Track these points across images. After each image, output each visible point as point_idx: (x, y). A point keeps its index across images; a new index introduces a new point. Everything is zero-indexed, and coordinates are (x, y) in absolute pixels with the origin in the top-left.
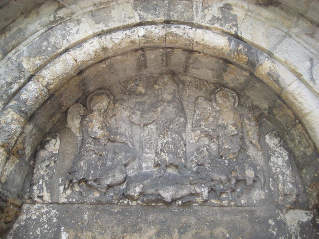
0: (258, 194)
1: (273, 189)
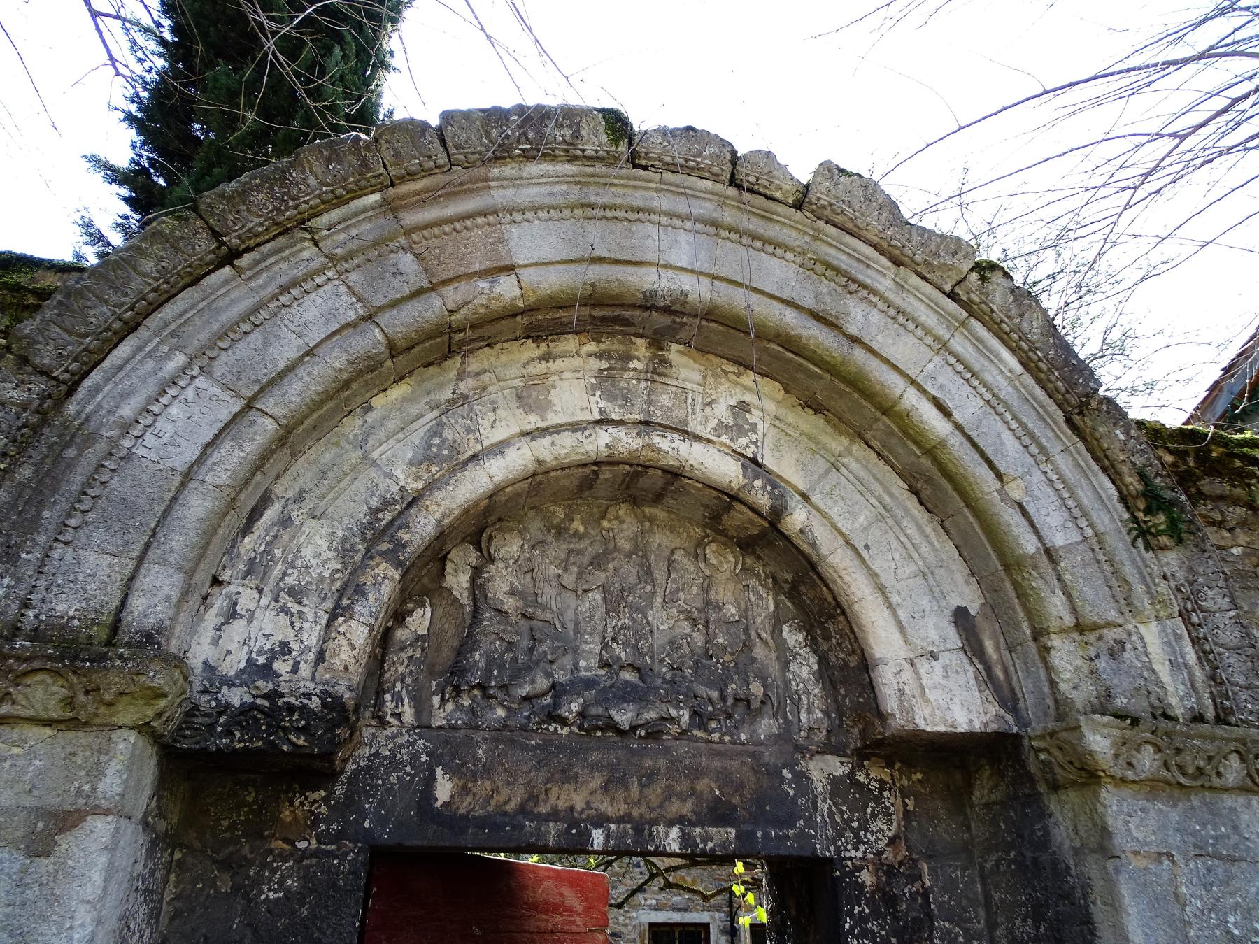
0: (767, 726)
1: (790, 717)
